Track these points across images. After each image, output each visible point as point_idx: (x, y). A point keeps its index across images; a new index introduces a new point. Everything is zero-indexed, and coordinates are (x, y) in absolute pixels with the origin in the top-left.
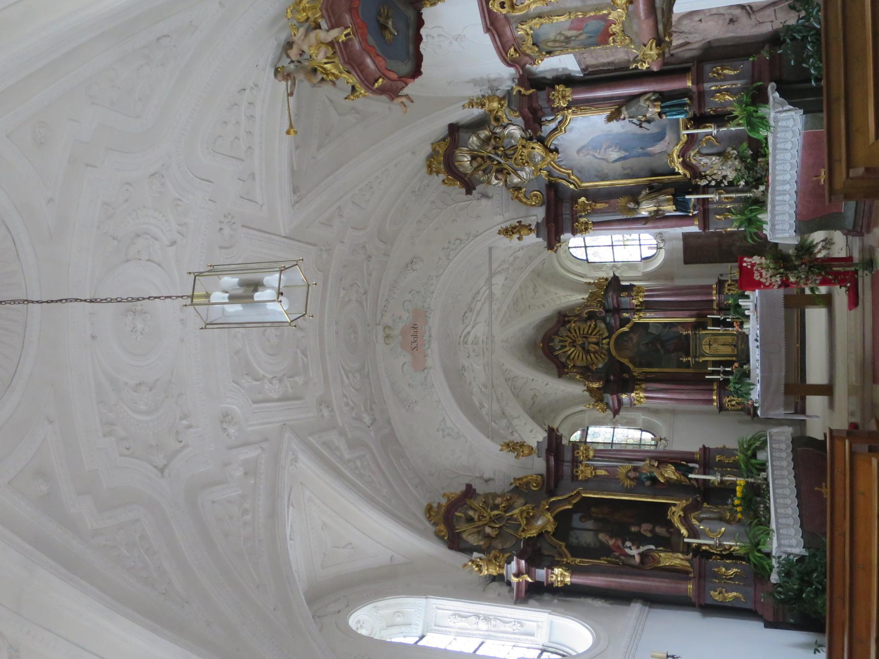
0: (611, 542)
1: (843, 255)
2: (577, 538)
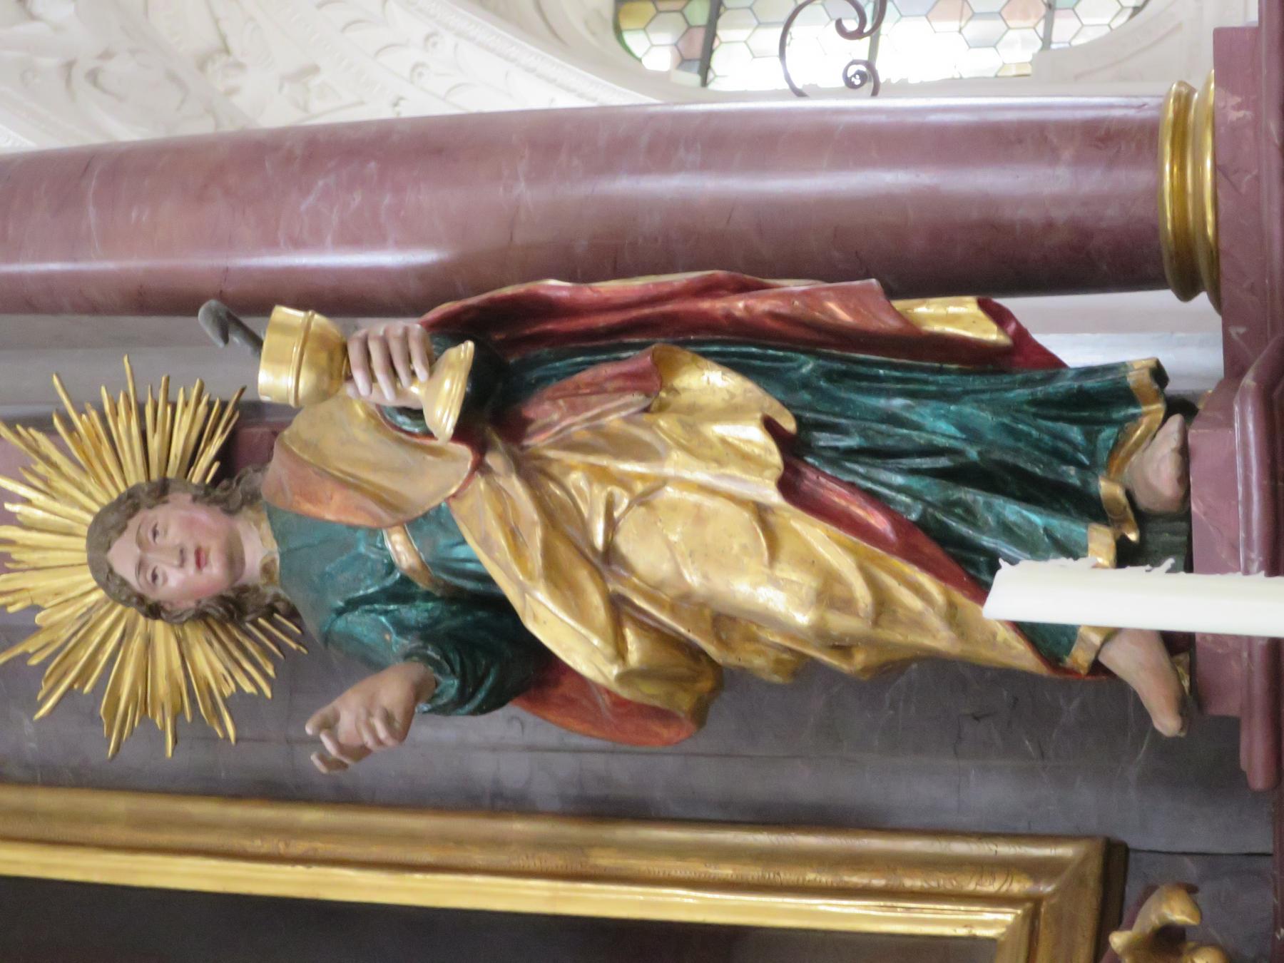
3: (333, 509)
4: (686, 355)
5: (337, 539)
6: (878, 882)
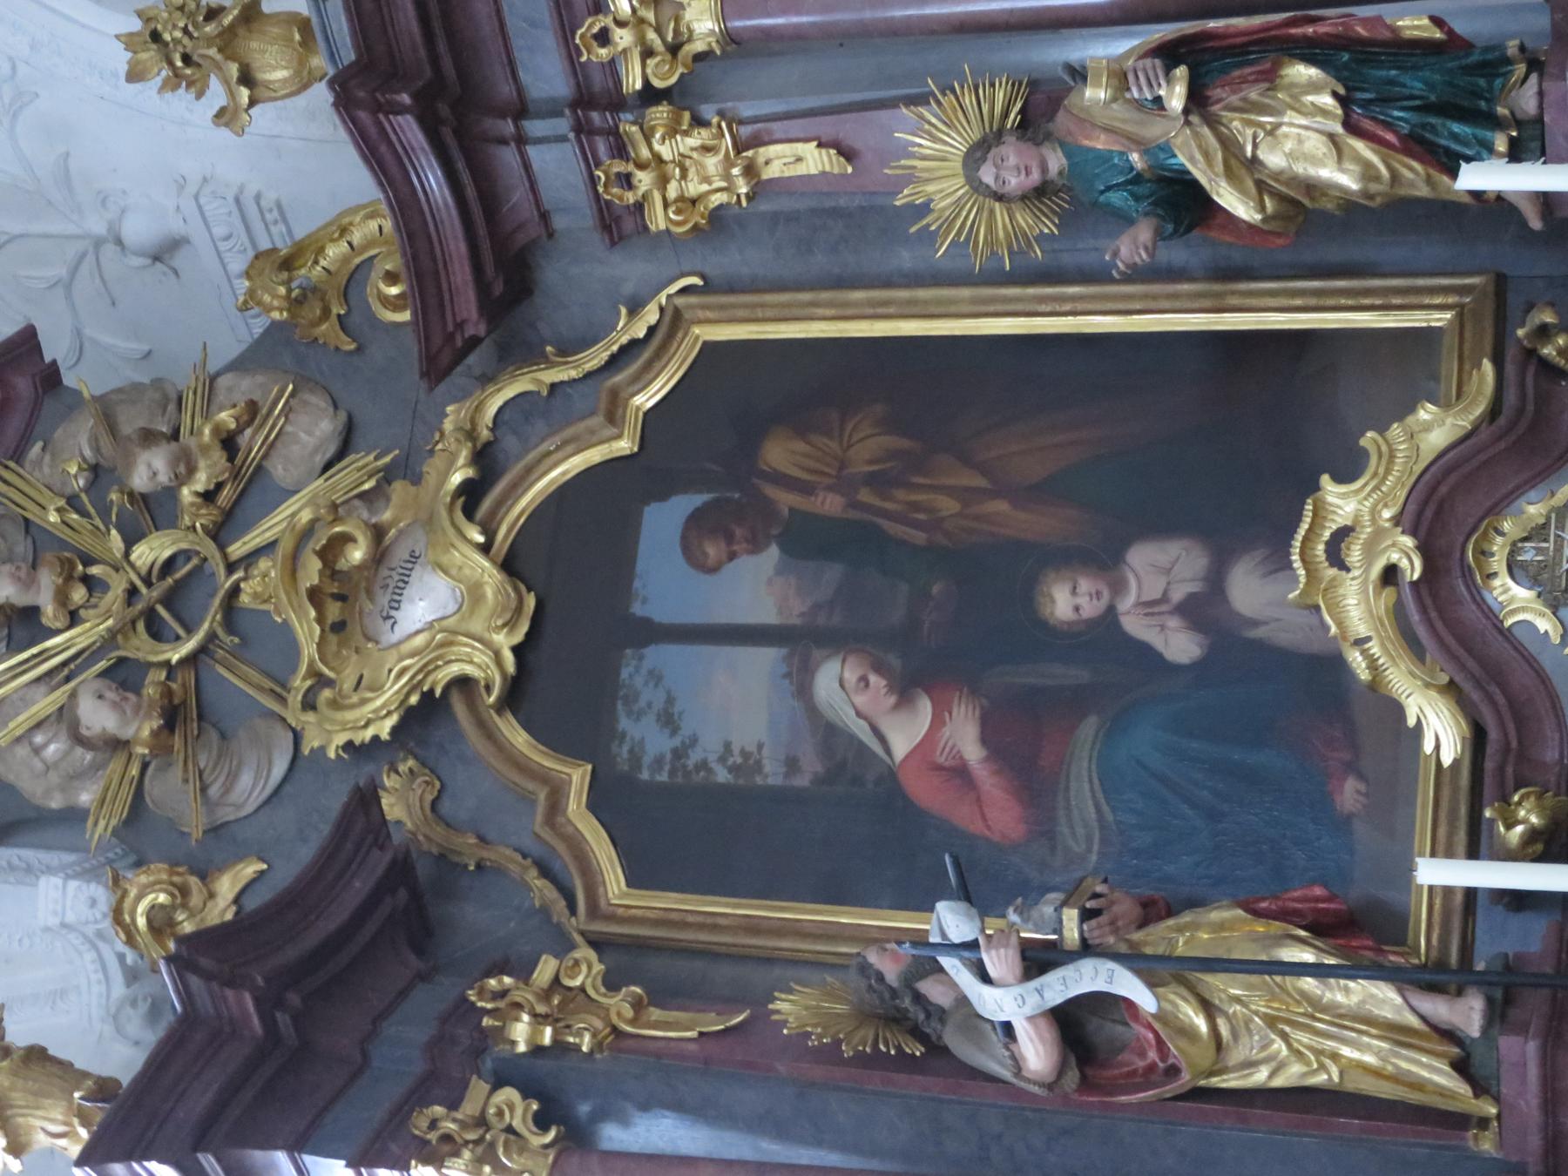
0: (904, 735)
1: (269, 246)
2: (669, 721)
3: (1100, 143)
4: (1286, 59)
5: (1104, 158)
6: (1378, 302)
